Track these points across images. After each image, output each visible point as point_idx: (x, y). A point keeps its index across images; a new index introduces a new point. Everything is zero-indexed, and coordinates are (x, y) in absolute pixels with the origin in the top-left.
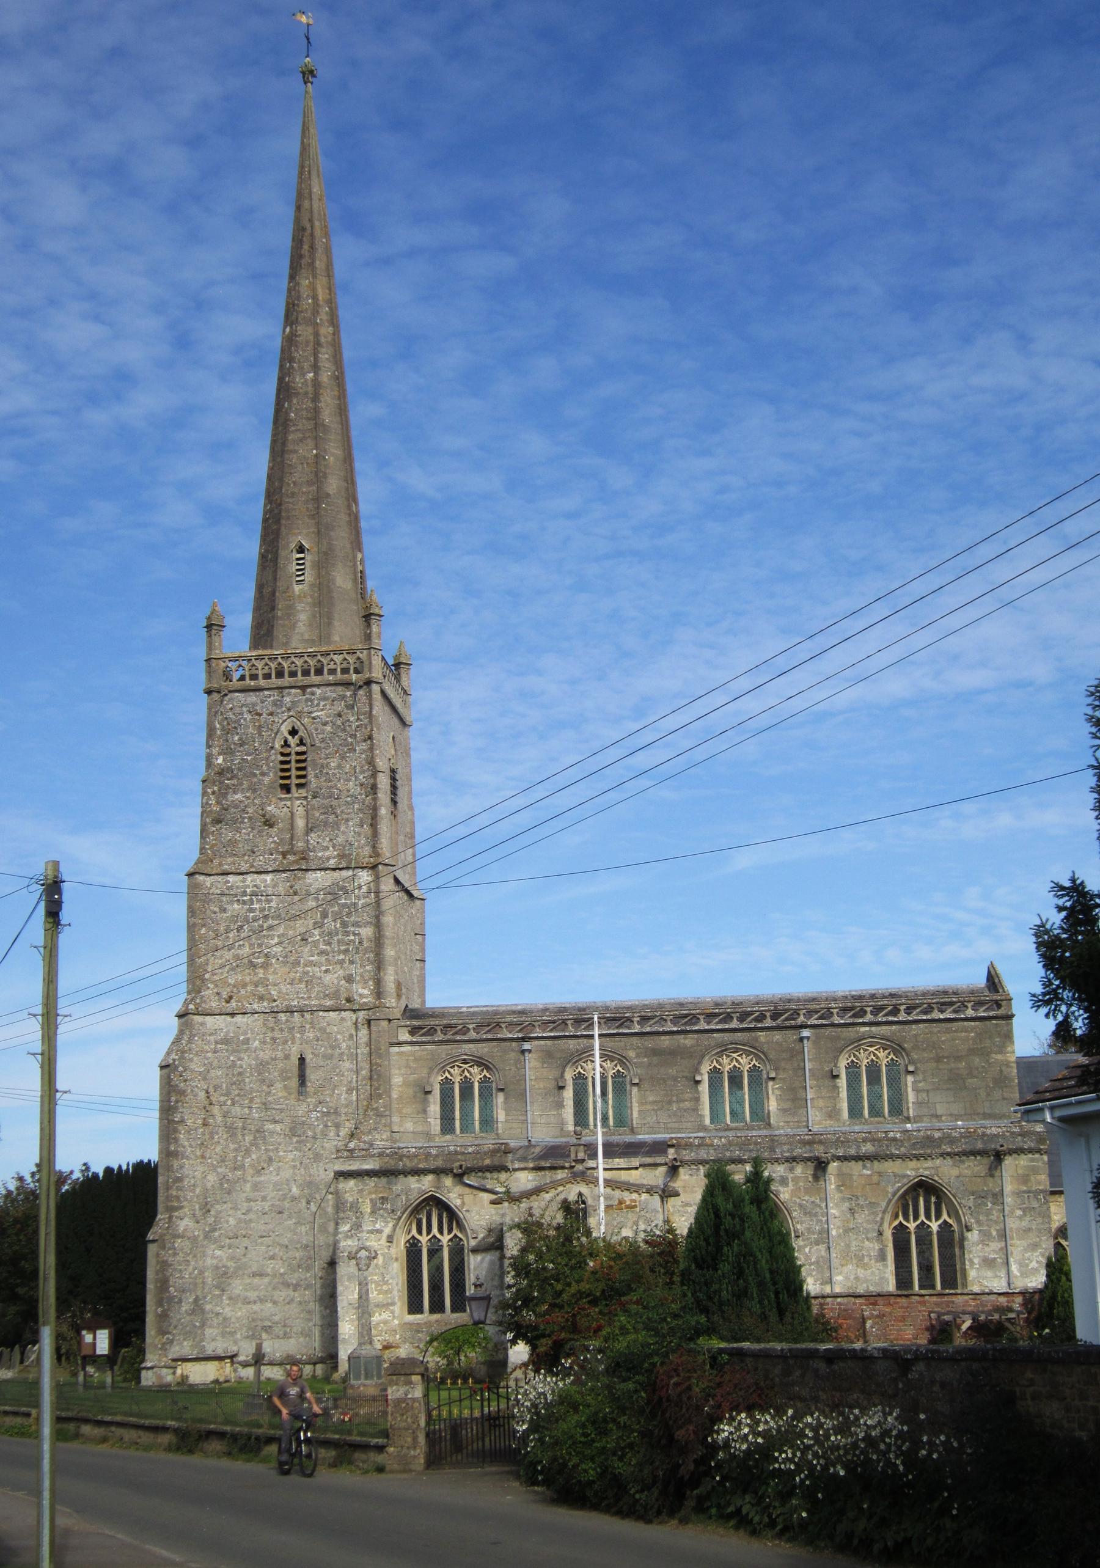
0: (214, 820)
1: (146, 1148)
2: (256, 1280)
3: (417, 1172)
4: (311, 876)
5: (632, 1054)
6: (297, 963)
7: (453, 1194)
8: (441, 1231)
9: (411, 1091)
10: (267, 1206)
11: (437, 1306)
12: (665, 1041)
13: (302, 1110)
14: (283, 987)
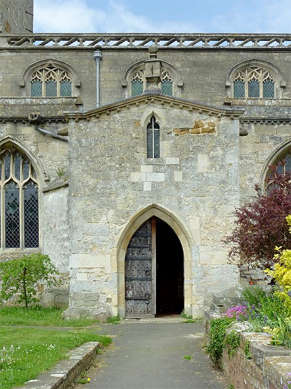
5: (178, 65)
7: (27, 138)
8: (17, 176)
9: (9, 86)
12: (204, 56)
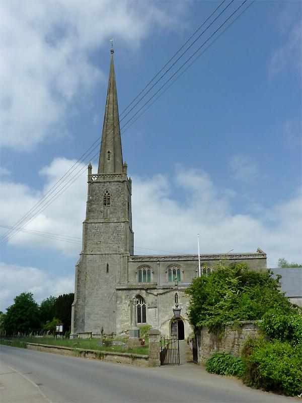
0: (89, 211)
1: (66, 286)
2: (96, 315)
3: (136, 289)
4: (110, 224)
6: (107, 243)
7: (143, 294)
10: (99, 298)
12: (189, 262)
13: (107, 276)
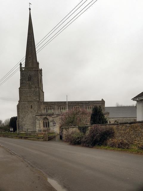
3: (44, 115)
7: (48, 117)
11: (46, 127)
14: (29, 99)
